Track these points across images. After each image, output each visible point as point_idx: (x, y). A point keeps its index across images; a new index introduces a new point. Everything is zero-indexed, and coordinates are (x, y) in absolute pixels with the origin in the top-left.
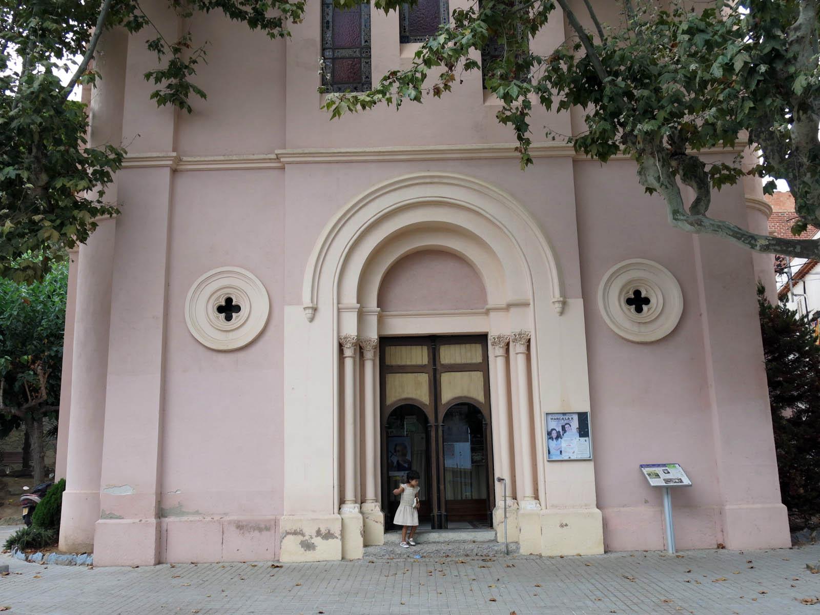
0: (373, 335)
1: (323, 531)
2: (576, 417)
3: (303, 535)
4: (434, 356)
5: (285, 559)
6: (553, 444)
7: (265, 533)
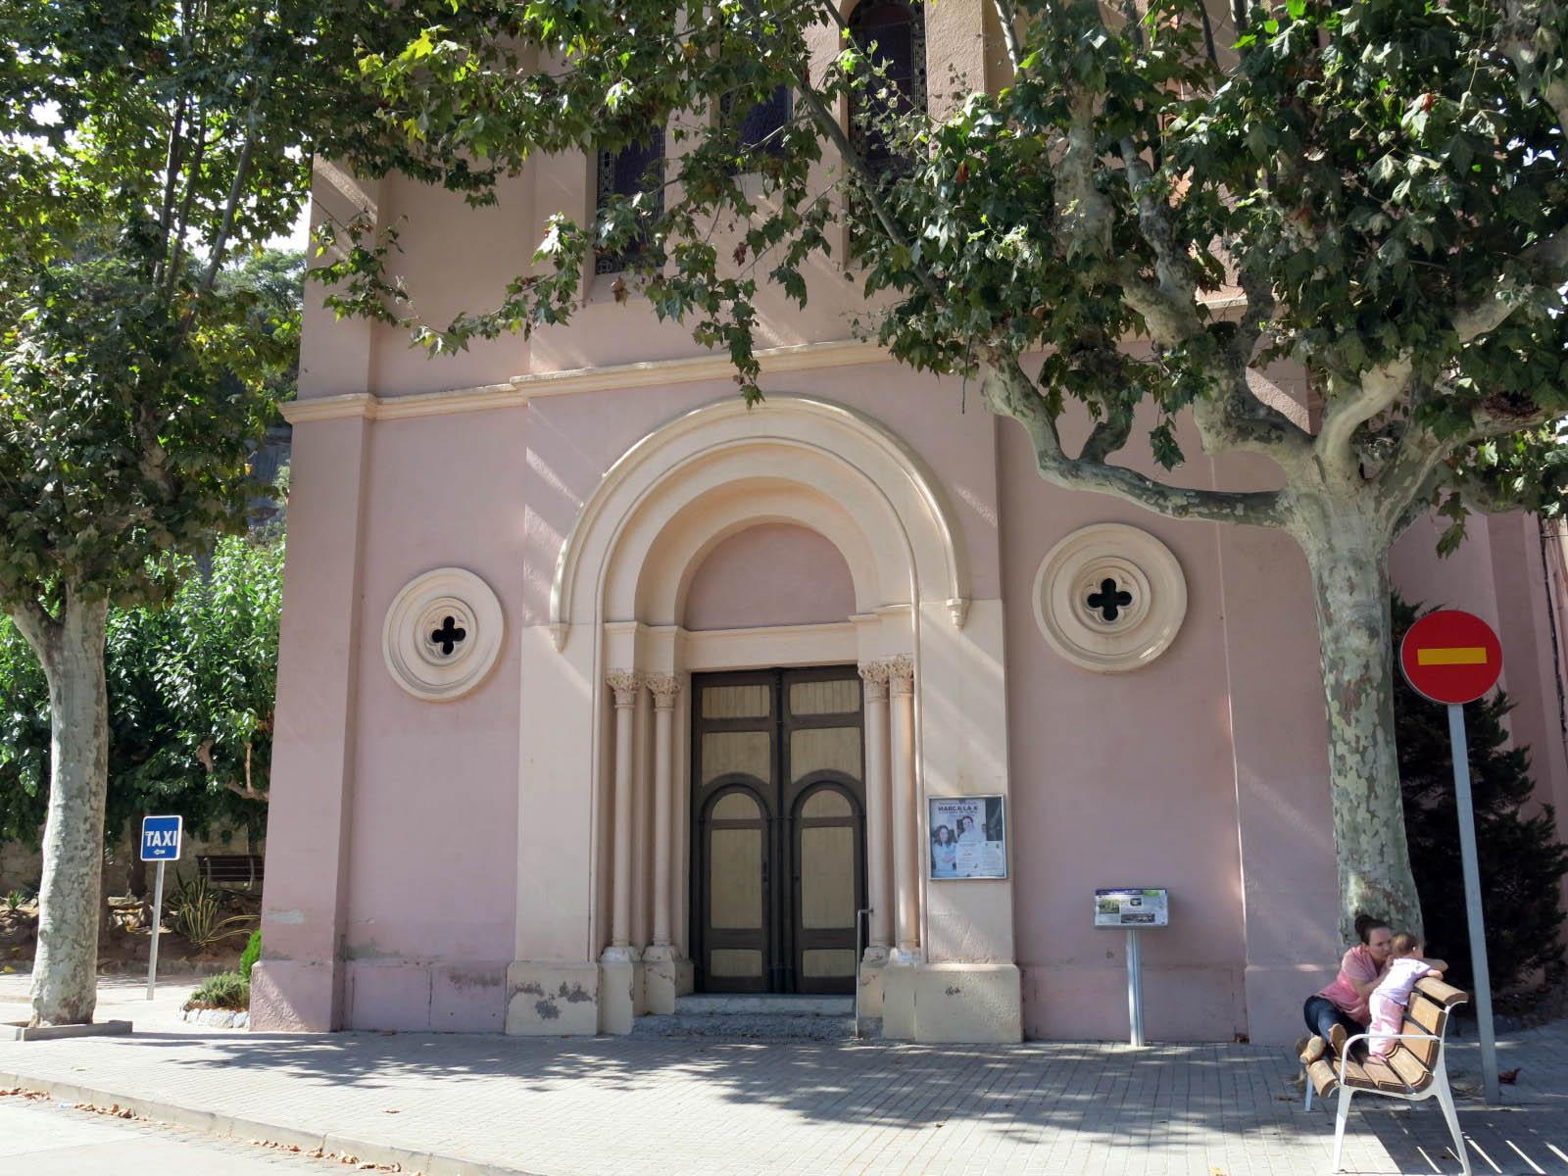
0: (665, 668)
1: (570, 987)
2: (982, 806)
3: (541, 993)
4: (780, 702)
5: (514, 1028)
6: (941, 851)
7: (491, 989)
